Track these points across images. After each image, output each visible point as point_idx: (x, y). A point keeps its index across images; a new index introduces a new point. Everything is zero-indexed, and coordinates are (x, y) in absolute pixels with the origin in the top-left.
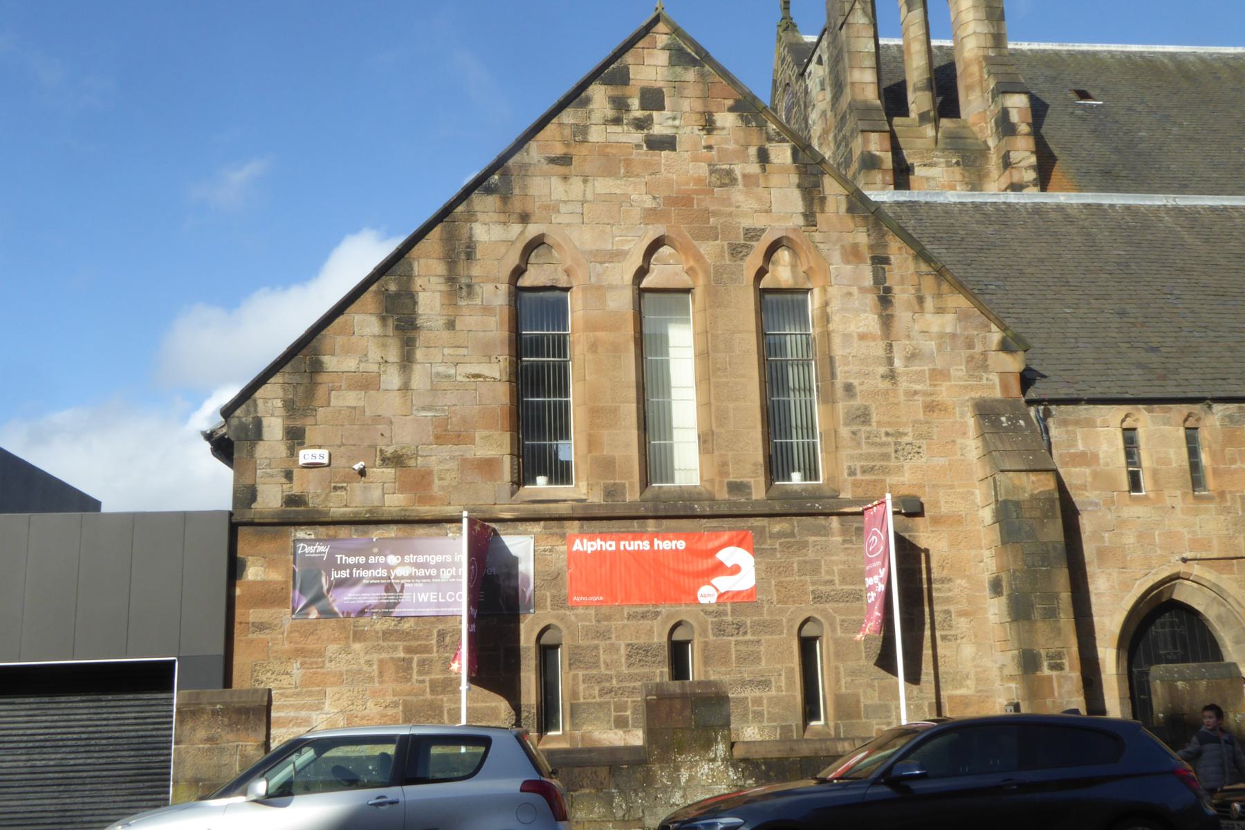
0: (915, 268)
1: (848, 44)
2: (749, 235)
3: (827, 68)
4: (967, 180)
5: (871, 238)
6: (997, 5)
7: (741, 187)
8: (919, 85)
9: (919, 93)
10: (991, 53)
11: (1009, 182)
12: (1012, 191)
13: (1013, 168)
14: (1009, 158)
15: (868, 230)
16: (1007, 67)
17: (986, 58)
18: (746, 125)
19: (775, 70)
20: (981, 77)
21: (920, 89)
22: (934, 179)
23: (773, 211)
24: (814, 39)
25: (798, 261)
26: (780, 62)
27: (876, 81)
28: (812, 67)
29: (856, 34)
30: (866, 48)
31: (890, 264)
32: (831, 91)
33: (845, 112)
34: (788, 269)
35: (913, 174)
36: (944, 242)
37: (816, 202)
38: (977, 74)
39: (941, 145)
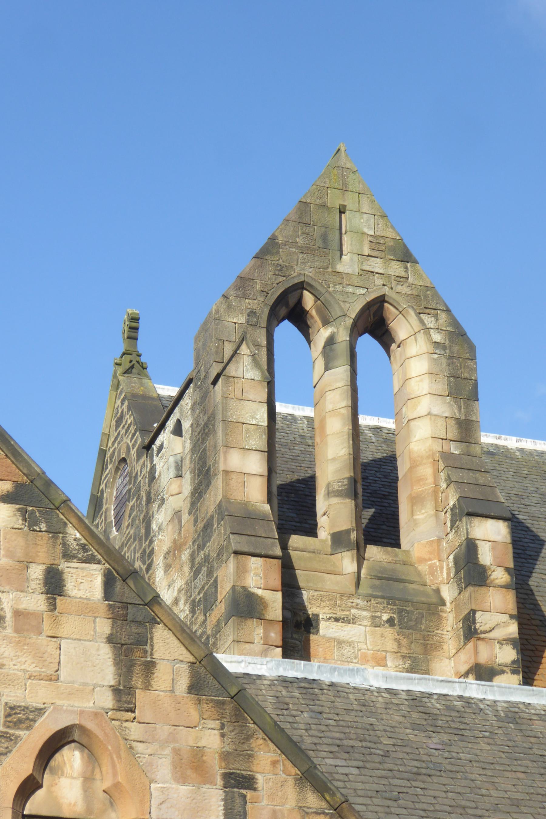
0: (298, 801)
1: (225, 409)
2: (14, 718)
3: (188, 441)
4: (404, 651)
5: (227, 740)
6: (466, 375)
7: (9, 631)
8: (336, 487)
9: (335, 500)
10: (455, 449)
11: (472, 662)
12: (477, 679)
13: (479, 639)
14: (474, 623)
15: (222, 727)
16: (478, 475)
17: (446, 456)
18: (29, 527)
19: (104, 434)
20: (437, 485)
21: (338, 494)
22: (350, 644)
23: (62, 678)
24: (172, 391)
25: (97, 770)
26: (114, 422)
27: (266, 473)
28: (165, 437)
29: (239, 395)
30: (253, 417)
31: (255, 789)
32: (193, 479)
33: (212, 517)
34: (78, 783)
35: (317, 632)
36: (357, 756)
37: (137, 669)
38: (431, 480)
39: (364, 589)
